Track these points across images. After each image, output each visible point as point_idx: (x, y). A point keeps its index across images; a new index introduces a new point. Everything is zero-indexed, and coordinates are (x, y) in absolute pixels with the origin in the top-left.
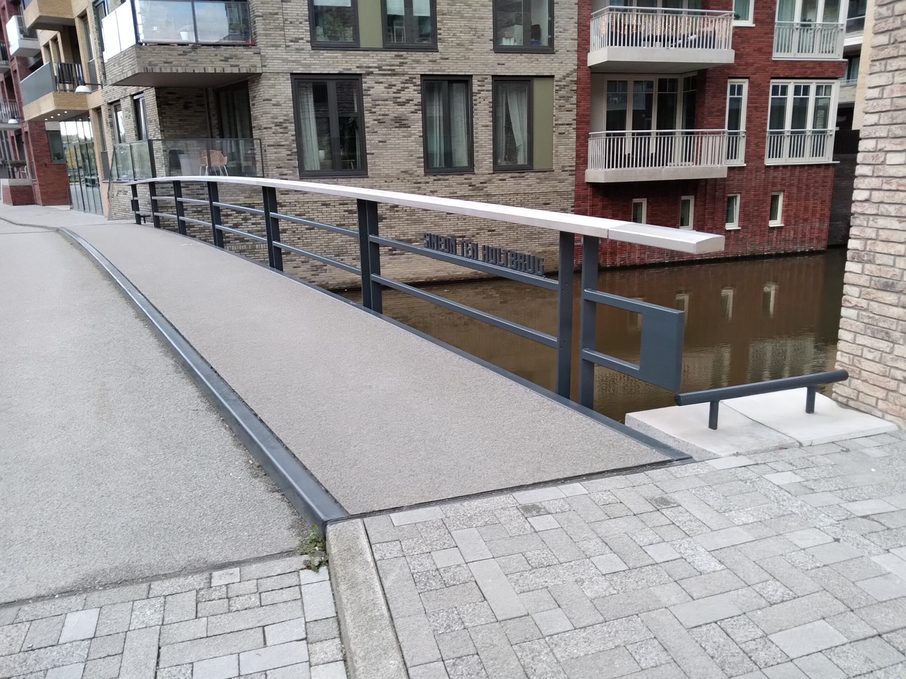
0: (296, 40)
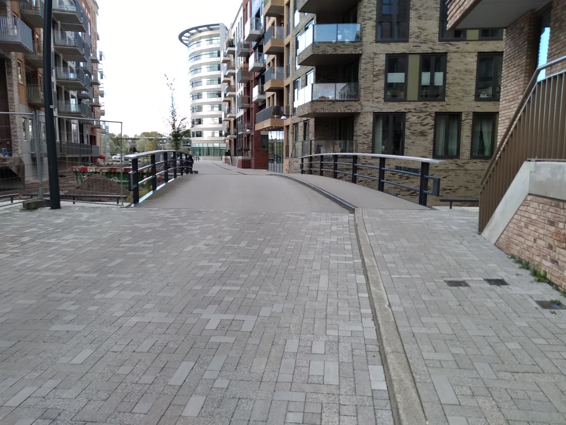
0: (377, 98)
